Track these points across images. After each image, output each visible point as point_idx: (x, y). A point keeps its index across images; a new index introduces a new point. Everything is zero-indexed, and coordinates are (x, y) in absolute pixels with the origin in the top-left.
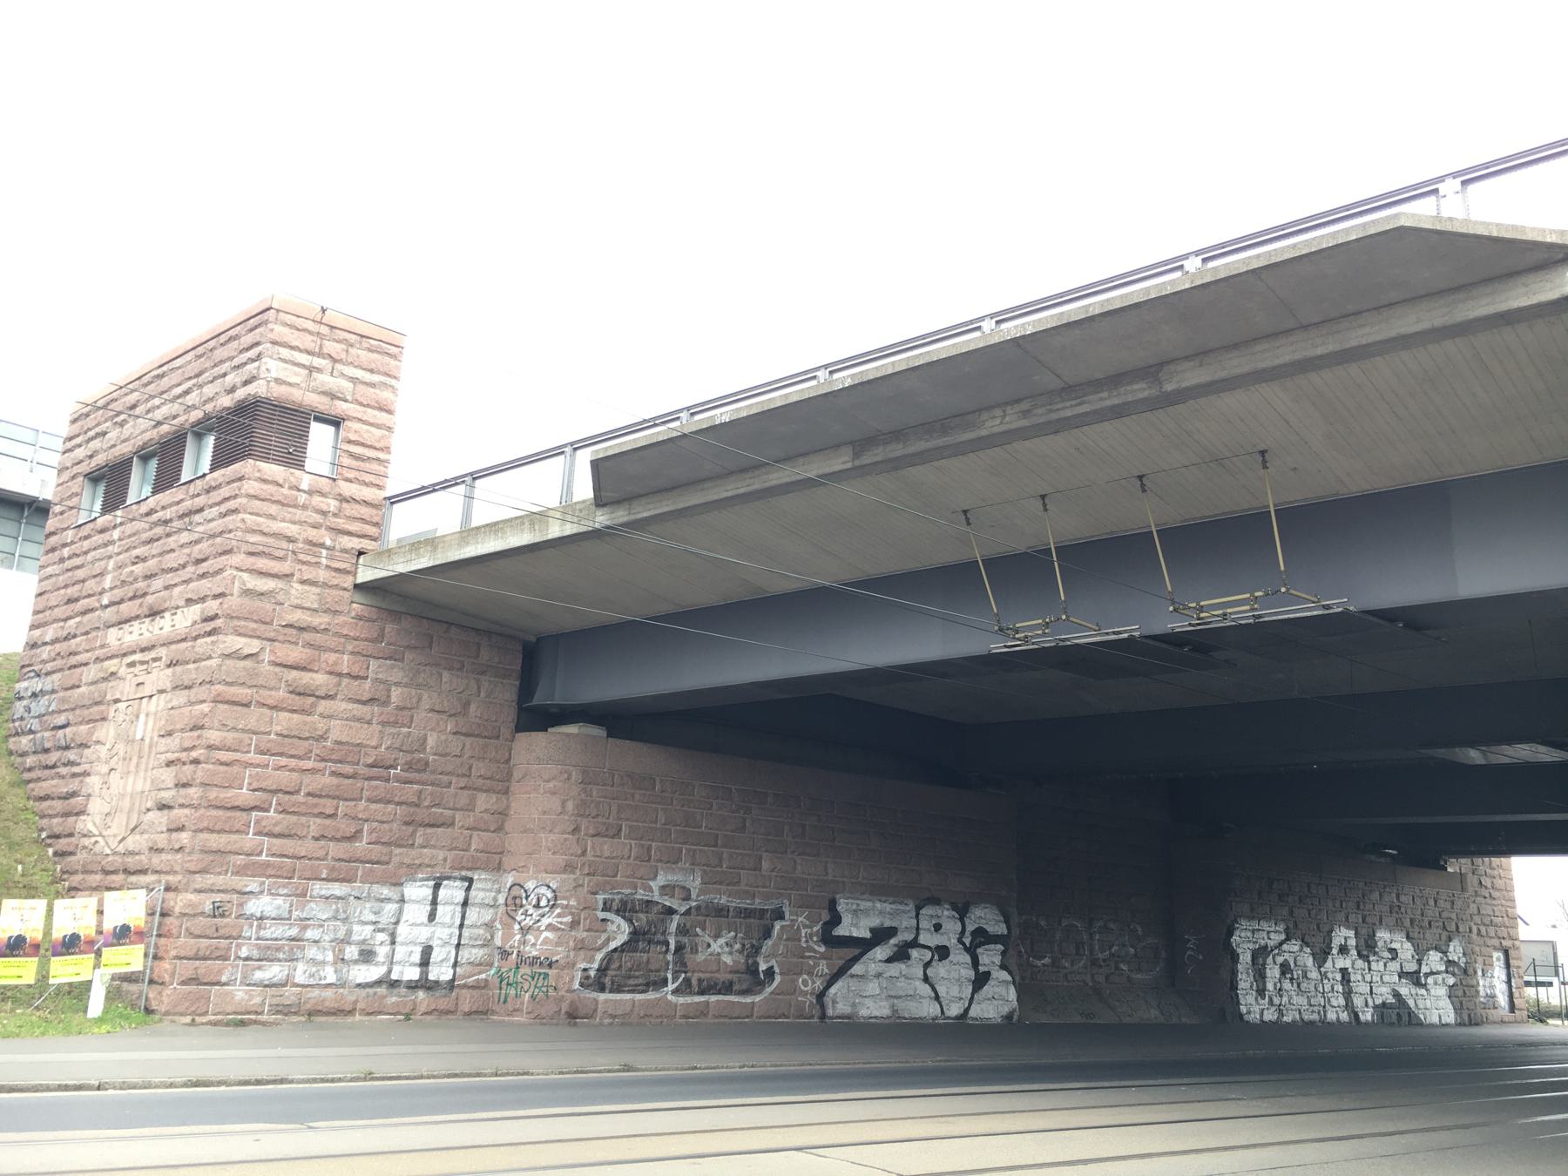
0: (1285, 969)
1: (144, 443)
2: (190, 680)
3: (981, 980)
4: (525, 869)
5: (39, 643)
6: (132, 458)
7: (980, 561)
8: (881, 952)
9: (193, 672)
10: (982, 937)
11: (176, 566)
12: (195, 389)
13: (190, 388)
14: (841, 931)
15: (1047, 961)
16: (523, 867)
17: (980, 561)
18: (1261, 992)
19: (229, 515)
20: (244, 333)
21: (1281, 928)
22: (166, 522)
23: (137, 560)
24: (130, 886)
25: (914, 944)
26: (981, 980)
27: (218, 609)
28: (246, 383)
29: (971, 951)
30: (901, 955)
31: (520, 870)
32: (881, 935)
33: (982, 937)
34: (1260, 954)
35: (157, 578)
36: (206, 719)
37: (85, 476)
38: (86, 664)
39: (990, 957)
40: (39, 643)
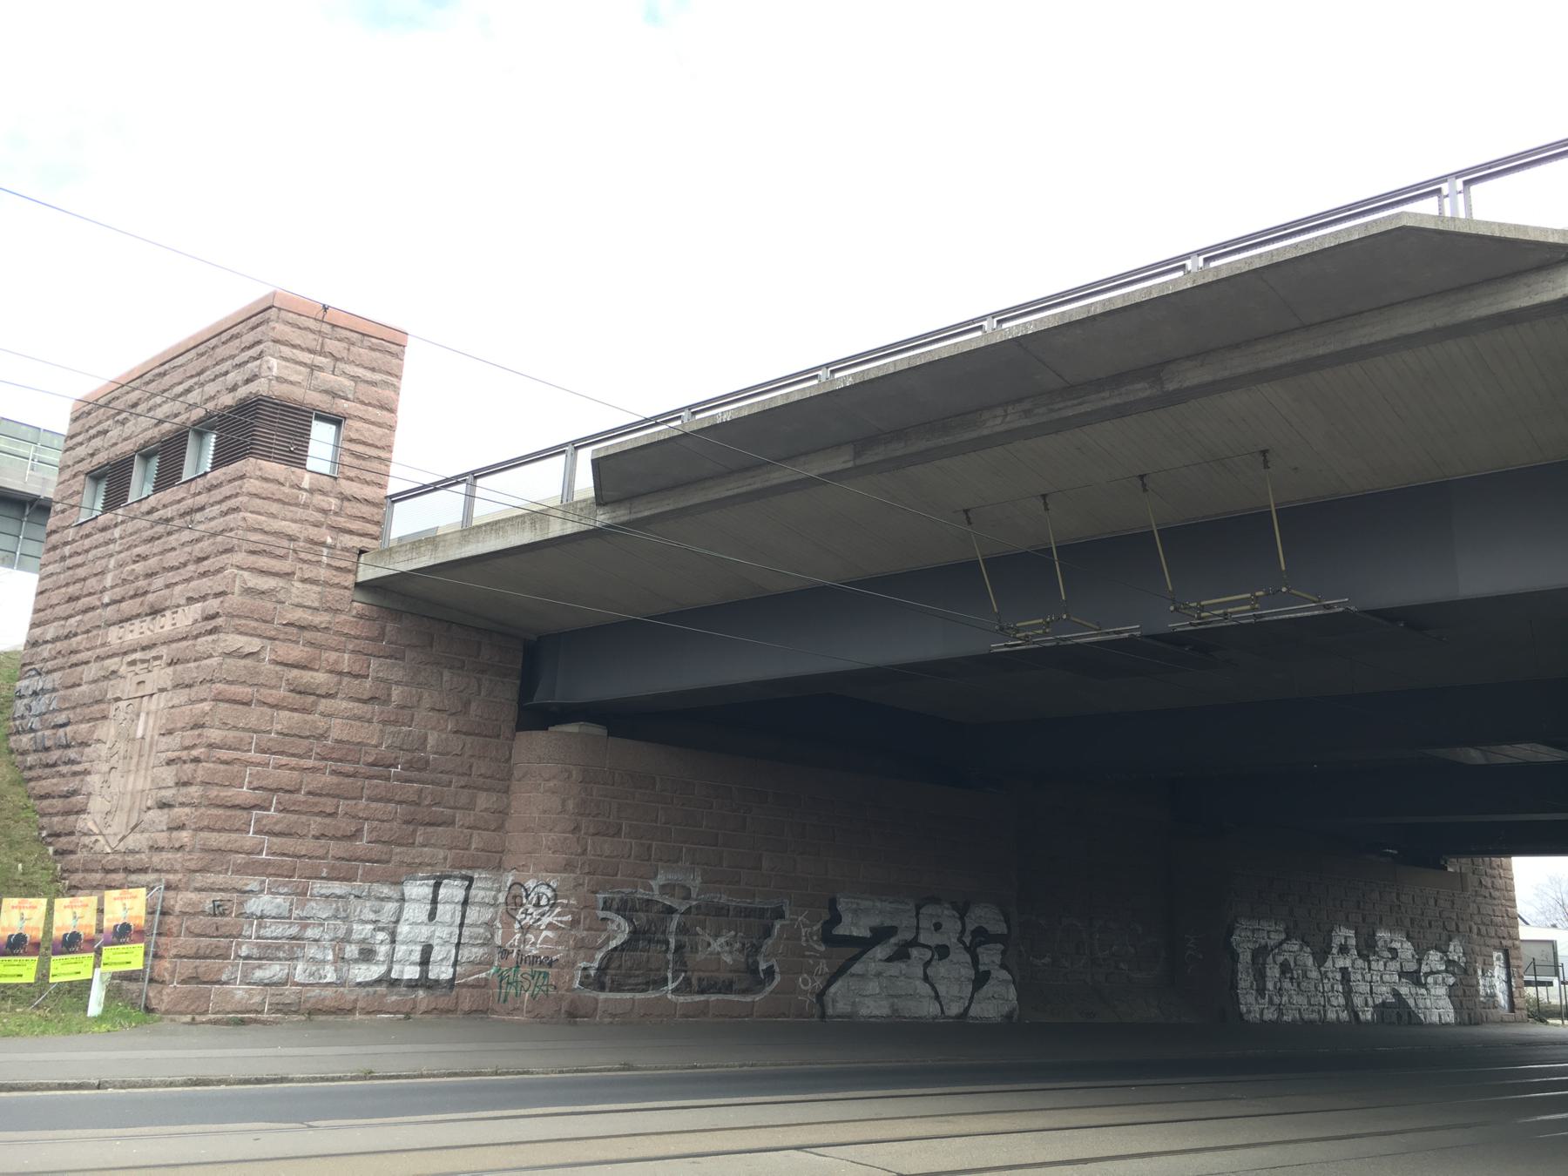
0: (1285, 968)
3: (981, 979)
4: (525, 869)
6: (134, 456)
7: (981, 561)
8: (880, 952)
10: (982, 936)
14: (840, 930)
15: (1047, 960)
17: (981, 561)
18: (1261, 991)
21: (1281, 927)
22: (168, 520)
23: (137, 559)
25: (914, 943)
26: (981, 979)
29: (971, 950)
30: (901, 954)
31: (521, 868)
32: (880, 935)
33: (982, 936)
34: (1260, 953)
36: (207, 718)
37: (87, 474)
38: (87, 663)
39: (990, 956)
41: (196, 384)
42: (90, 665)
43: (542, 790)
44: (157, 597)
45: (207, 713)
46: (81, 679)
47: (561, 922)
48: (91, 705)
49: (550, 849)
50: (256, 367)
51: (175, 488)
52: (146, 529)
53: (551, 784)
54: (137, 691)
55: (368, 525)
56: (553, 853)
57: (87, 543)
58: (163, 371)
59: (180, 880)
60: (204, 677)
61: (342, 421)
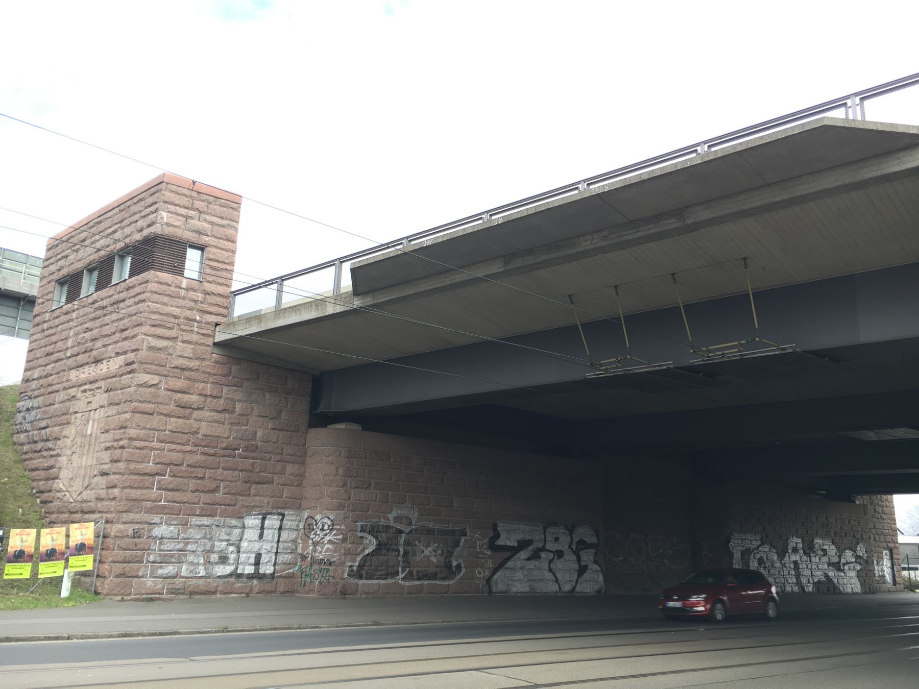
6: (83, 270)
11: (110, 333)
12: (119, 229)
13: (117, 229)
16: (314, 506)
22: (103, 308)
23: (86, 330)
27: (134, 358)
31: (312, 508)
36: (128, 423)
37: (56, 281)
38: (58, 391)
40: (31, 379)
41: (119, 228)
43: (324, 462)
47: (336, 539)
49: (329, 497)
54: (87, 407)
59: (114, 518)
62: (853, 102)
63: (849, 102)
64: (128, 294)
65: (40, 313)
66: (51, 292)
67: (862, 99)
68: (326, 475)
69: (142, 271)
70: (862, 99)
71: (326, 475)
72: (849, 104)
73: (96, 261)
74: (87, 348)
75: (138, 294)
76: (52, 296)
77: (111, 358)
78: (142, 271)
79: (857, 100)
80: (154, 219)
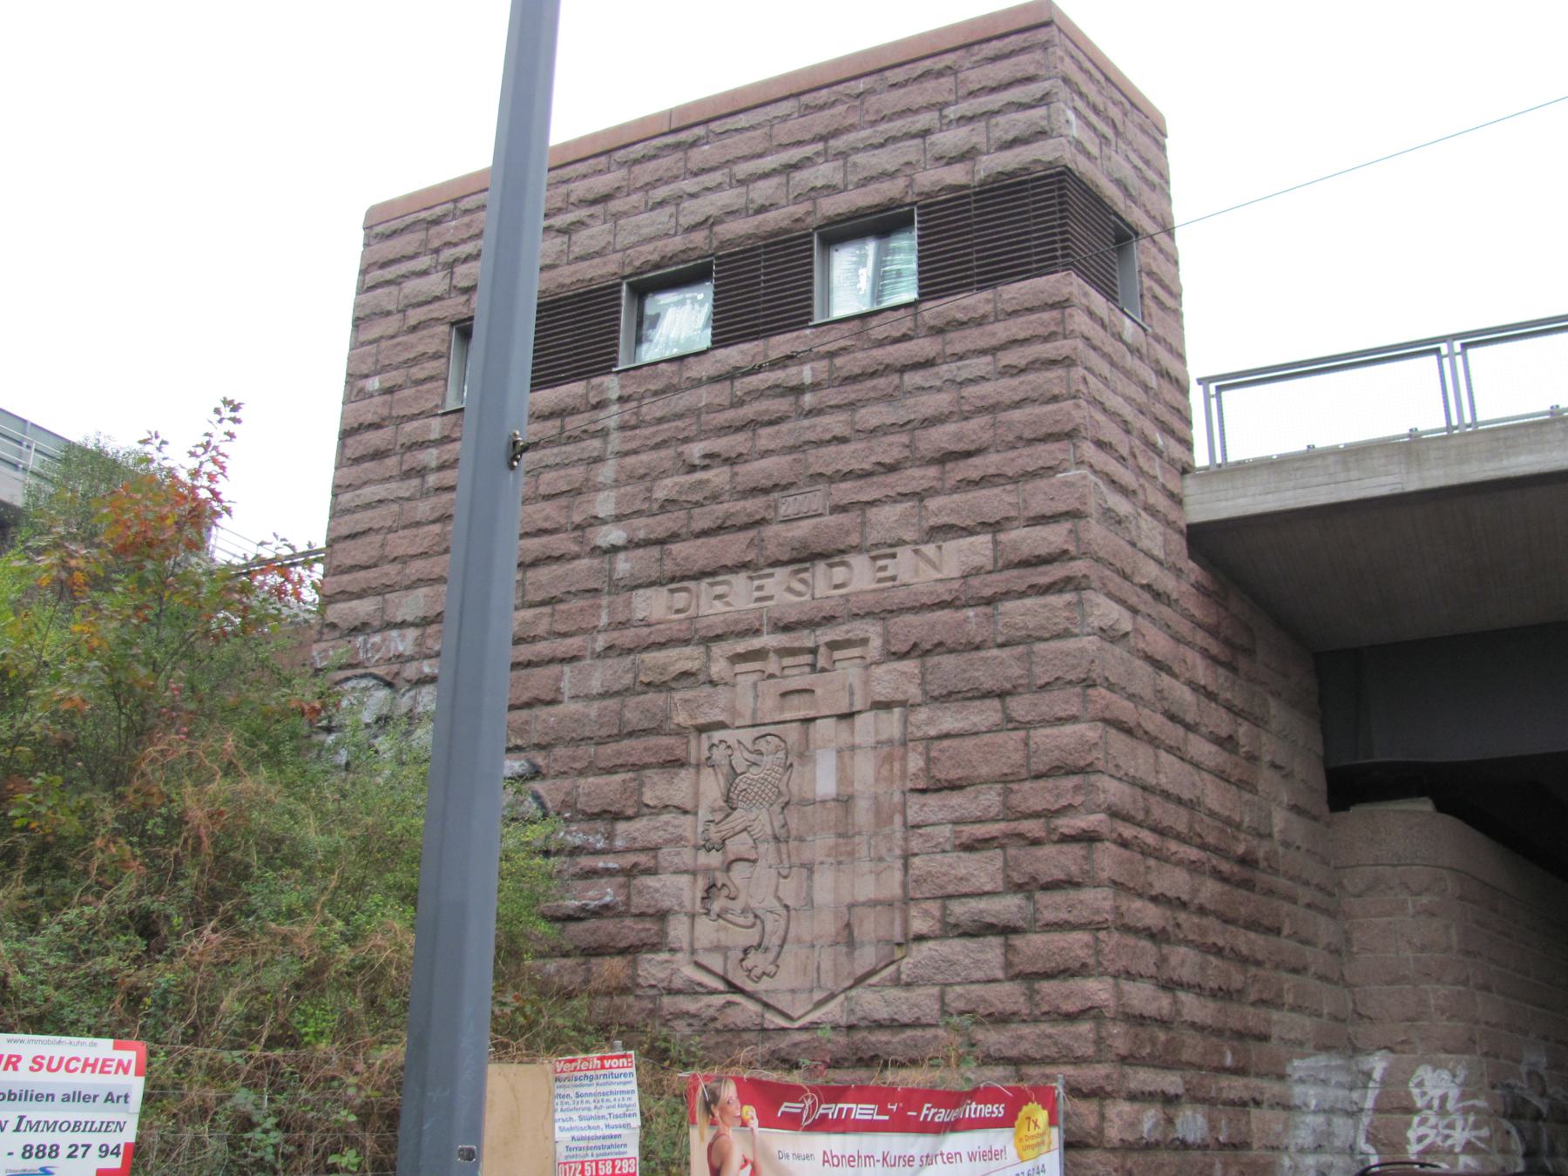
1: (663, 258)
2: (1008, 679)
4: (1407, 1047)
5: (376, 623)
6: (619, 285)
9: (254, 859)
11: (867, 466)
12: (821, 160)
13: (808, 158)
16: (1403, 1042)
19: (1038, 370)
20: (968, 65)
22: (798, 390)
23: (707, 462)
24: (659, 1125)
27: (1066, 542)
28: (442, 467)
31: (1398, 1048)
35: (792, 491)
36: (1095, 754)
37: (452, 324)
38: (574, 659)
40: (376, 623)
41: (817, 154)
42: (582, 664)
43: (1411, 910)
44: (815, 527)
45: (1096, 744)
46: (558, 690)
47: (1479, 1139)
48: (611, 738)
49: (1443, 1013)
50: (1042, 118)
51: (808, 332)
52: (721, 408)
53: (1425, 900)
54: (782, 709)
55: (357, 516)
56: (1449, 1019)
57: (1130, 362)
58: (690, 139)
59: (1108, 1077)
60: (1060, 673)
61: (1130, 238)
62: (1451, 348)
63: (1444, 348)
64: (945, 344)
65: (383, 419)
66: (436, 356)
67: (1465, 346)
68: (1423, 949)
69: (779, 327)
70: (1465, 346)
71: (1423, 949)
72: (1444, 350)
73: (694, 255)
74: (729, 516)
75: (1015, 341)
76: (443, 368)
77: (901, 542)
78: (779, 327)
79: (1457, 345)
80: (1044, 123)
